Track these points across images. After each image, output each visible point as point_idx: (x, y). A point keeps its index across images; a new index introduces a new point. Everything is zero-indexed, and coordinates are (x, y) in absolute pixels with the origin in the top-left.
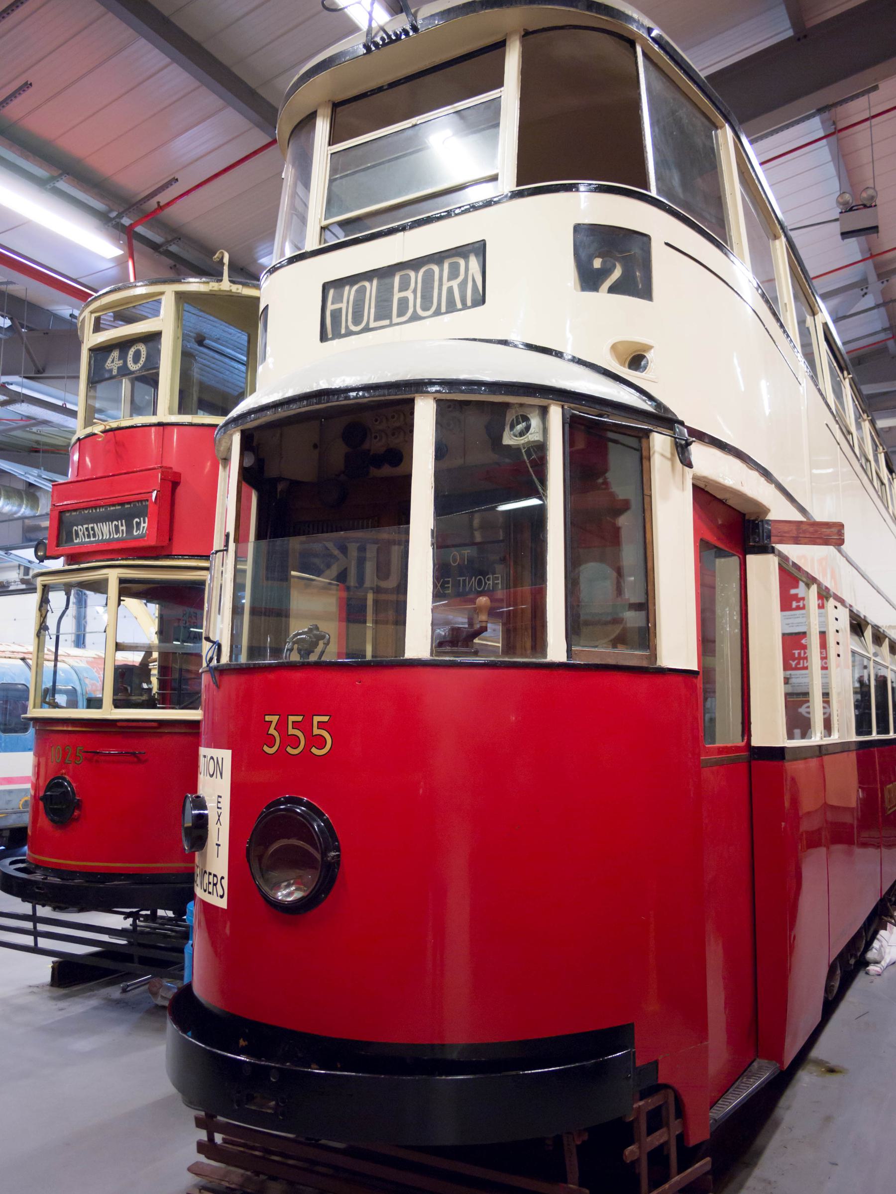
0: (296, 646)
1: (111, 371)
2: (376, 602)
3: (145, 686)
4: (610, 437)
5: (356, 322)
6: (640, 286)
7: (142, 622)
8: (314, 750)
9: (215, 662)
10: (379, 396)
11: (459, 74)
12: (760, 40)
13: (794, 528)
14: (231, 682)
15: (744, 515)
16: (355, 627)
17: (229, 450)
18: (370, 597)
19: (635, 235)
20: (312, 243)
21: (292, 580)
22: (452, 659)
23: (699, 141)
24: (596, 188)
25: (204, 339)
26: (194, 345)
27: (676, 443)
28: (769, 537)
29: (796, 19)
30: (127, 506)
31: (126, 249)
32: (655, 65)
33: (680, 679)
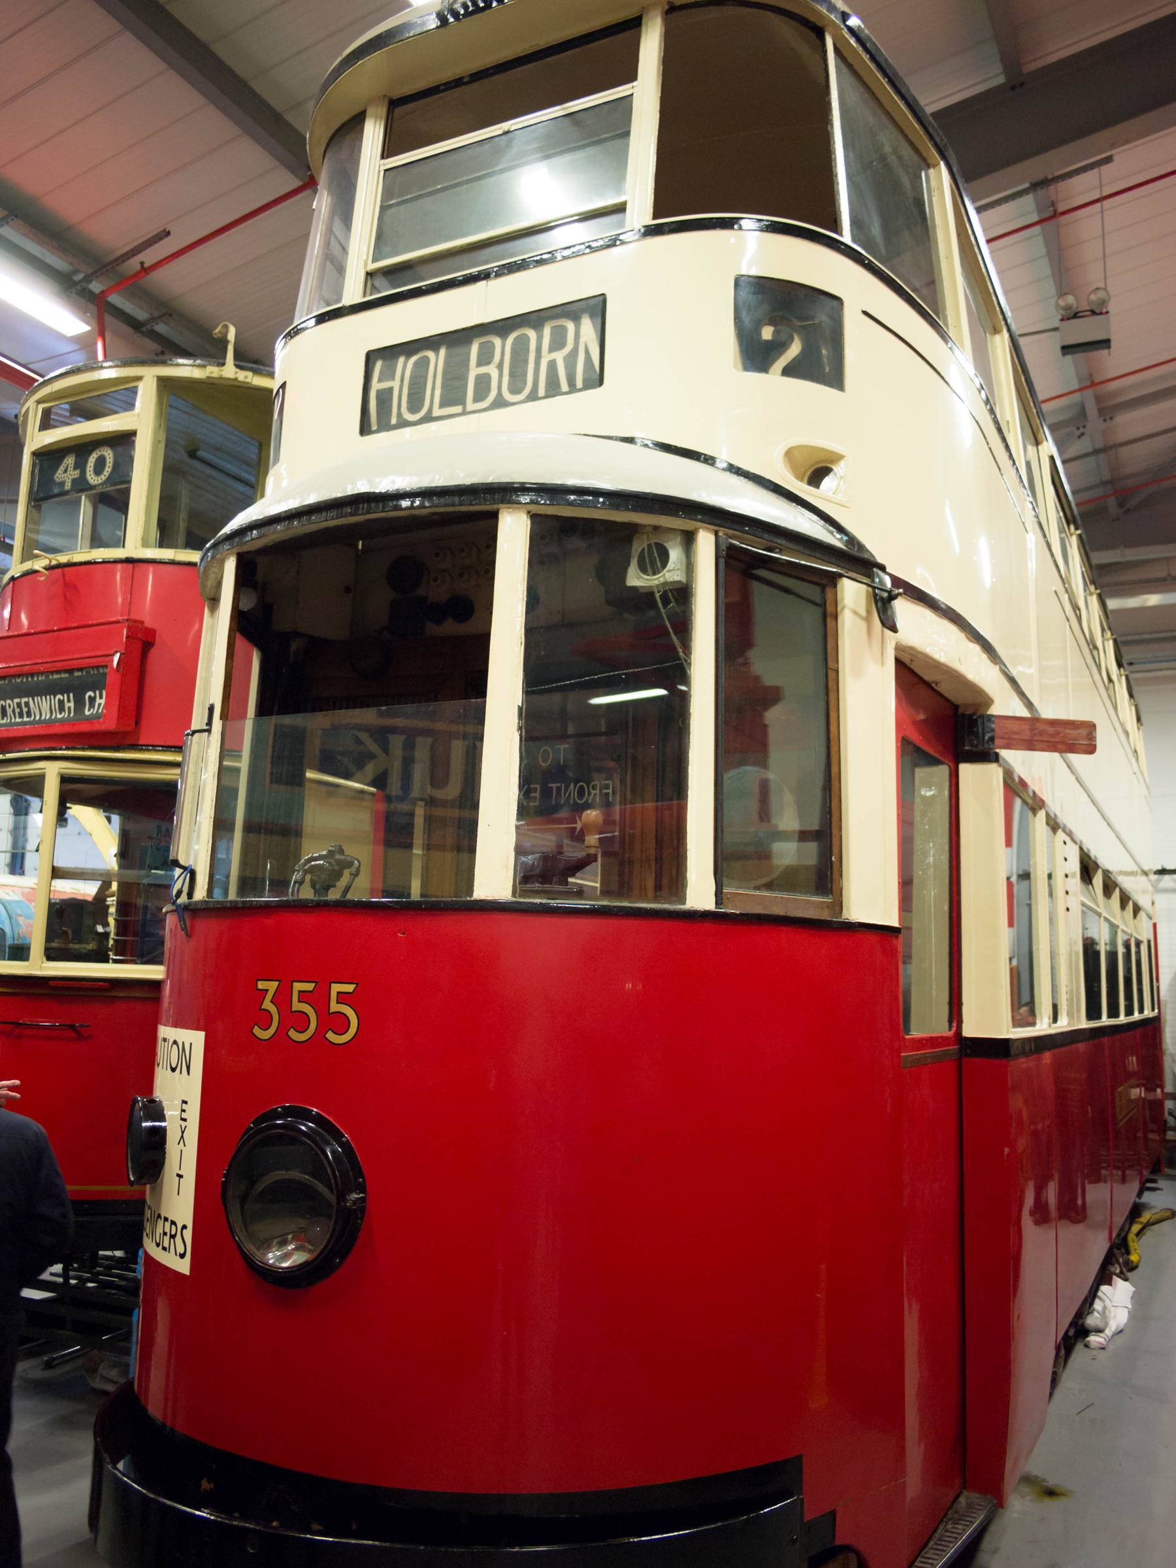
0: (308, 877)
1: (63, 484)
2: (428, 819)
3: (100, 929)
4: (789, 578)
5: (414, 408)
6: (827, 370)
7: (97, 836)
8: (330, 1036)
9: (183, 899)
10: (446, 505)
11: (573, 65)
12: (955, 90)
13: (1026, 727)
14: (207, 928)
15: (956, 707)
16: (396, 854)
17: (219, 584)
18: (420, 812)
19: (822, 297)
20: (353, 293)
21: (307, 784)
22: (544, 901)
23: (905, 181)
24: (767, 226)
25: (196, 450)
26: (182, 461)
27: (875, 595)
28: (992, 739)
29: (1011, 62)
30: (77, 674)
31: (94, 323)
32: (850, 66)
33: (873, 938)
